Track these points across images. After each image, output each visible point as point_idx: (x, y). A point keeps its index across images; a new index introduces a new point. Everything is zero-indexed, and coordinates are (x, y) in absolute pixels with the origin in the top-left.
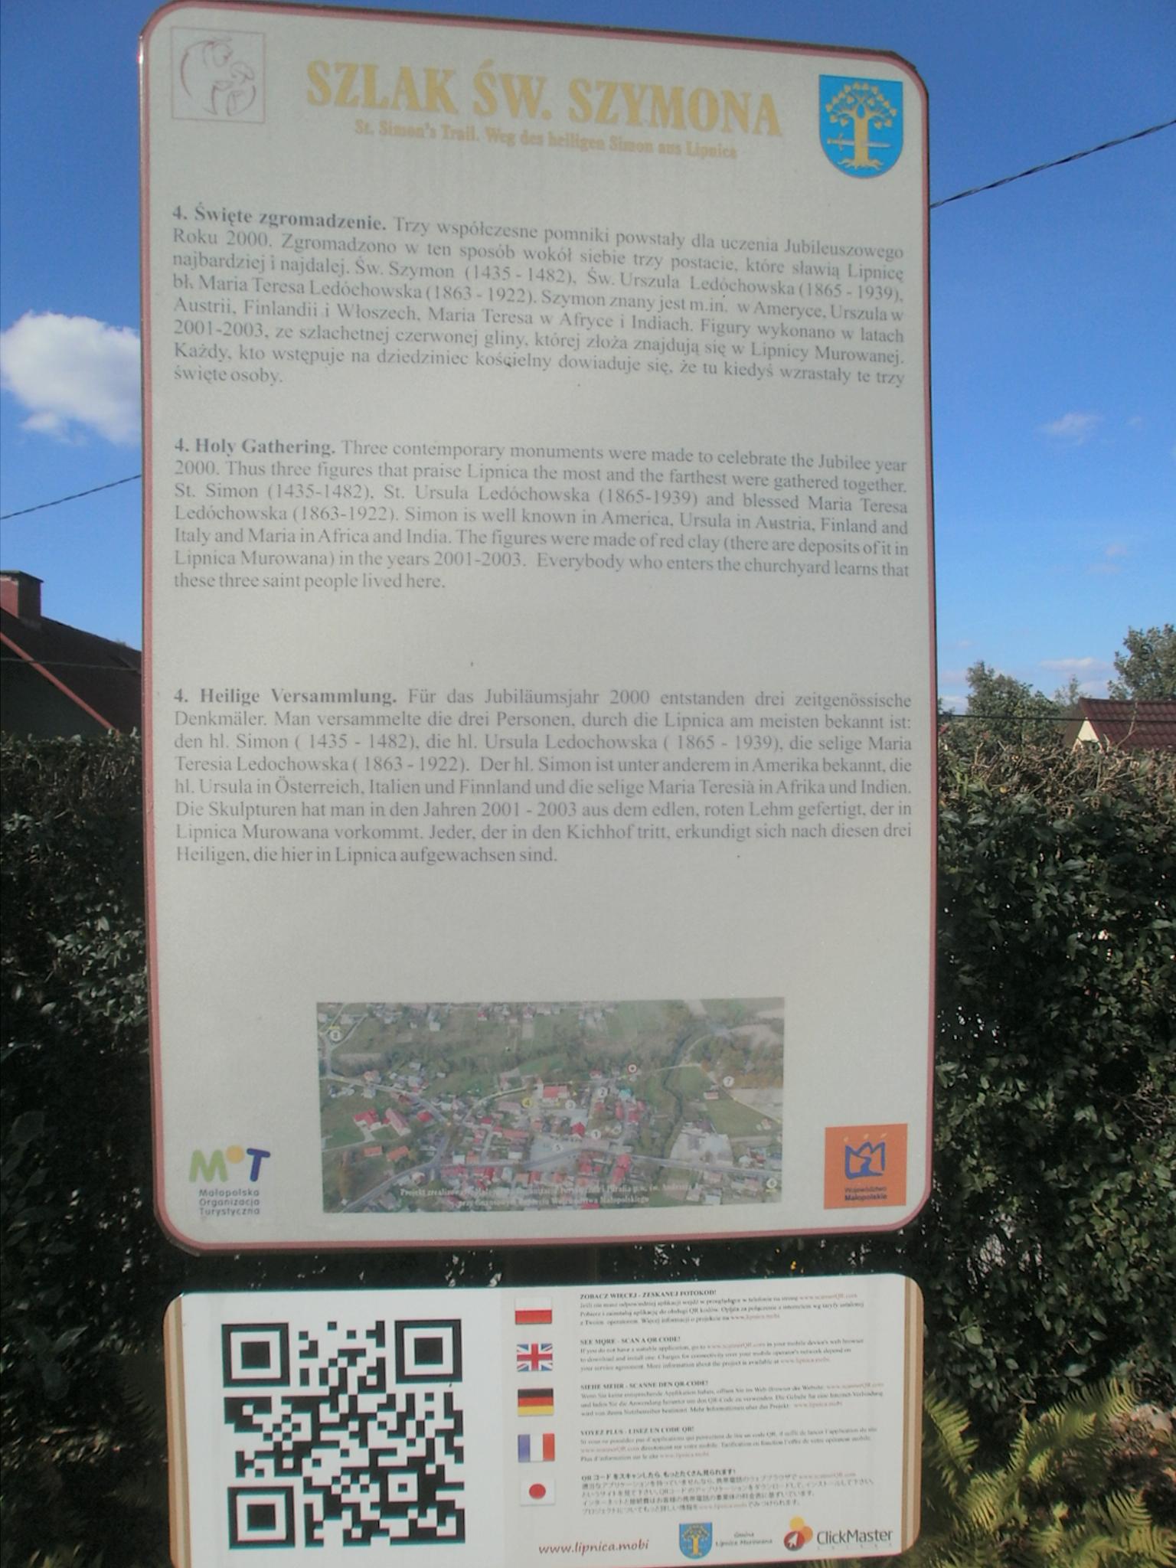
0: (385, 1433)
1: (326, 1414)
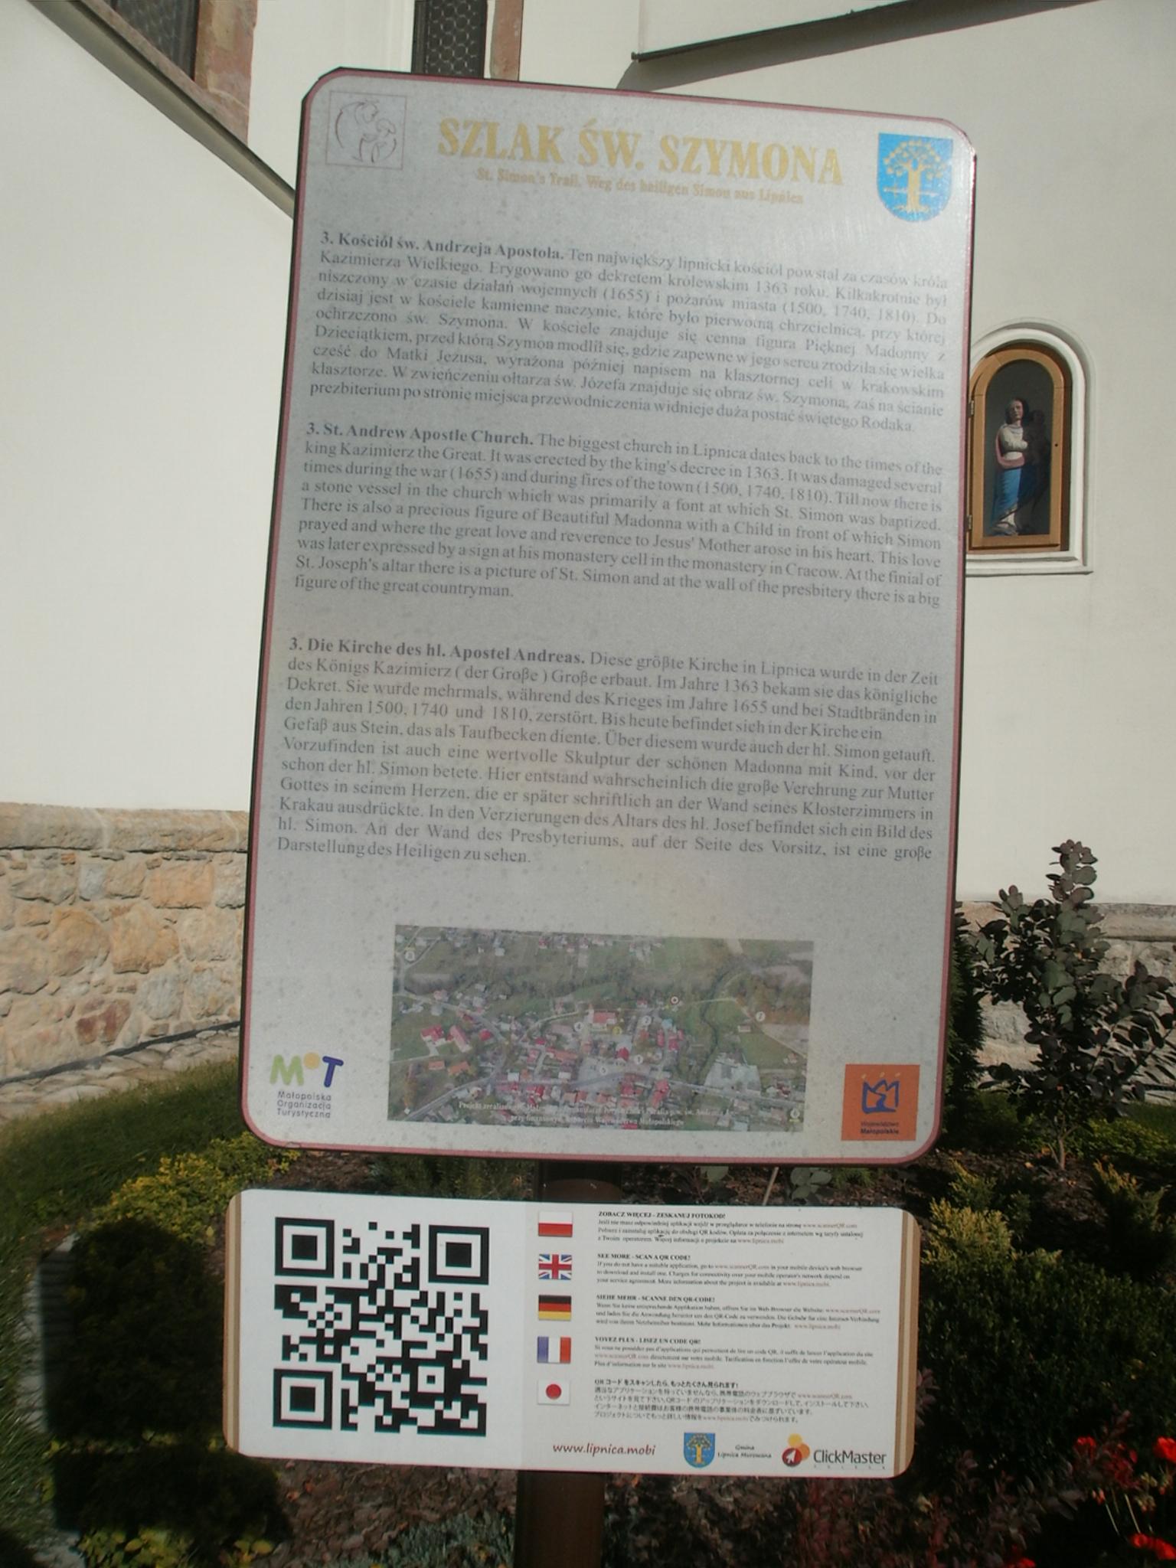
0: (416, 1327)
1: (365, 1306)
